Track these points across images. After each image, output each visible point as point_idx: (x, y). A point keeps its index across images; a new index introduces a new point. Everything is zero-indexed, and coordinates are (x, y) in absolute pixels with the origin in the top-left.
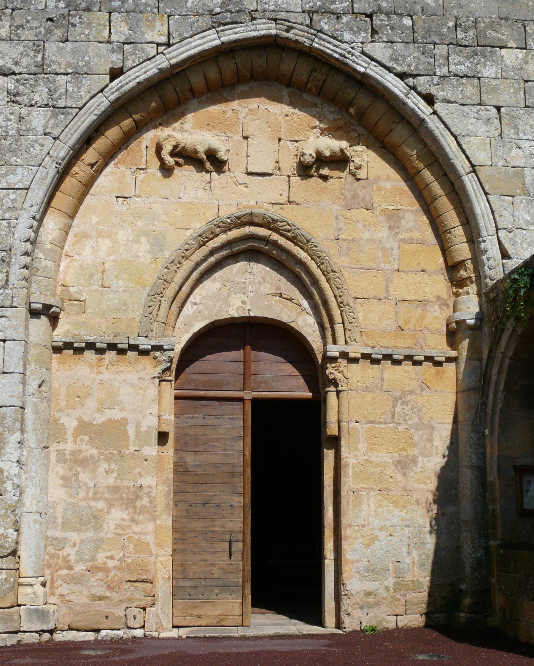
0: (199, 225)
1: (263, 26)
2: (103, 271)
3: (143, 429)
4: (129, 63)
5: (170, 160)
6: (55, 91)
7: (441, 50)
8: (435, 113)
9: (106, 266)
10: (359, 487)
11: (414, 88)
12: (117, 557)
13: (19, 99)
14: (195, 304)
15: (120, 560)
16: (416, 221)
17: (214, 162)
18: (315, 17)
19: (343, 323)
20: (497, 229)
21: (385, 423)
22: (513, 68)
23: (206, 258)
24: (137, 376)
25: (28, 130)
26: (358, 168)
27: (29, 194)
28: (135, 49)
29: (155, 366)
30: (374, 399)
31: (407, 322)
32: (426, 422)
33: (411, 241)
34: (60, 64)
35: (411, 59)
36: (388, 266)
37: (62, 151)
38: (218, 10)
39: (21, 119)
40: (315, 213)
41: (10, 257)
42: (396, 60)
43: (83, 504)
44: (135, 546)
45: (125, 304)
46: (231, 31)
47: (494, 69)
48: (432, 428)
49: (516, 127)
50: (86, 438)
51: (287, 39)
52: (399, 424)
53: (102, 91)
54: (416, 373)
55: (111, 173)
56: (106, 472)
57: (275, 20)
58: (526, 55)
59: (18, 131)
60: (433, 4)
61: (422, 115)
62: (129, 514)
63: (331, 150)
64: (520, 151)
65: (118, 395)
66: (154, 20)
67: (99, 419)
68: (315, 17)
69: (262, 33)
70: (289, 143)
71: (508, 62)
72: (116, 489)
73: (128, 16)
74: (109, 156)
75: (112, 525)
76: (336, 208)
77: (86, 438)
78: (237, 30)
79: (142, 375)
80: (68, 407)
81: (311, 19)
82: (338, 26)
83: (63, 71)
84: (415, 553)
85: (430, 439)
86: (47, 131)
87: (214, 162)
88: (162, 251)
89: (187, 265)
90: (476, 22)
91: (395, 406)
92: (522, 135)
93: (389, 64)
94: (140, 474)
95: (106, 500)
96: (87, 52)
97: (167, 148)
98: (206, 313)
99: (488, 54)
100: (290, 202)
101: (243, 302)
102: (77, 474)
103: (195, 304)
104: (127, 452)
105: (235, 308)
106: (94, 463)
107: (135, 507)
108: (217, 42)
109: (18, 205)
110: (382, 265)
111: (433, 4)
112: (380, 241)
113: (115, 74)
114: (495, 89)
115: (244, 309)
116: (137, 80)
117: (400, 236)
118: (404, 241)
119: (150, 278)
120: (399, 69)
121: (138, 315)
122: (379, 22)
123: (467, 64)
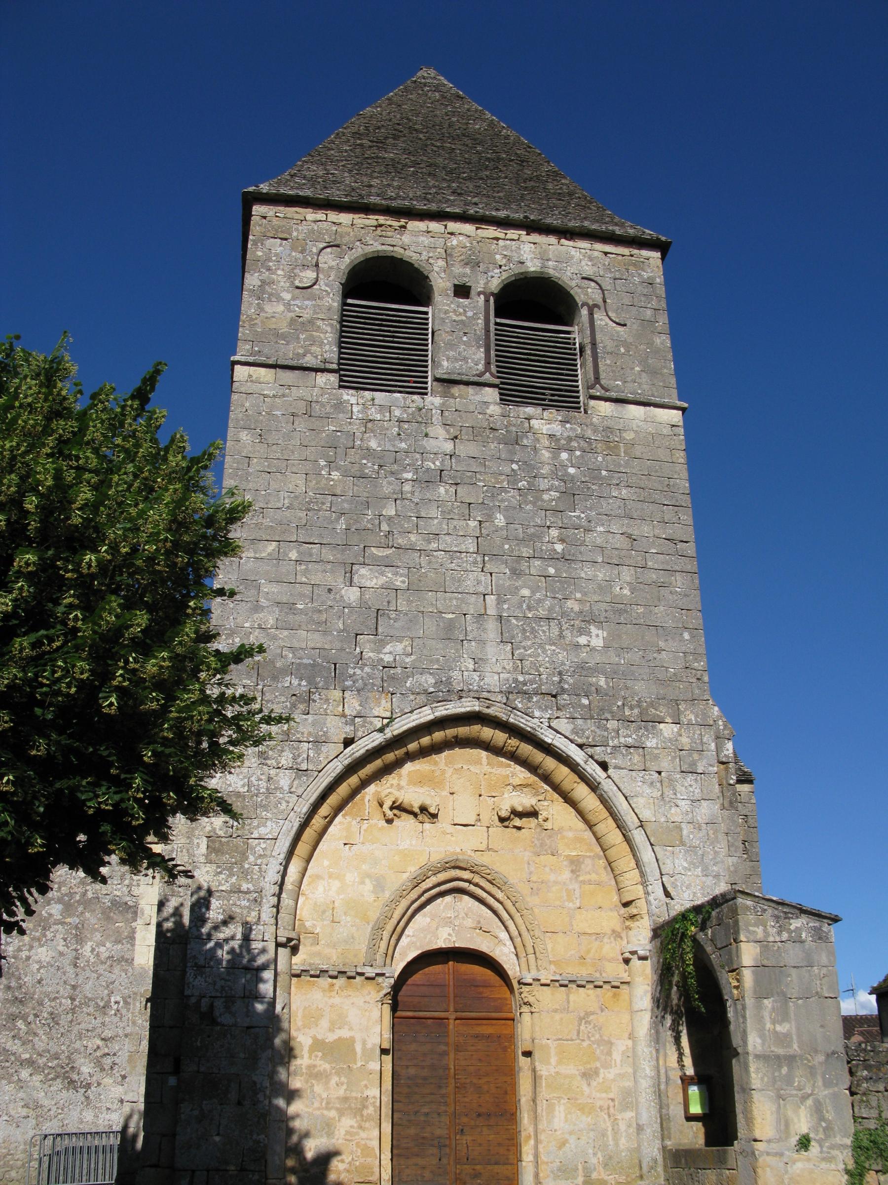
0: (412, 869)
1: (469, 704)
2: (333, 908)
3: (369, 1046)
4: (360, 734)
5: (390, 814)
6: (299, 756)
7: (612, 724)
8: (609, 777)
9: (336, 904)
10: (551, 1096)
11: (591, 757)
12: (347, 1161)
13: (269, 762)
14: (408, 936)
15: (350, 1163)
16: (593, 865)
17: (425, 813)
18: (511, 697)
19: (535, 953)
20: (662, 875)
21: (572, 1040)
22: (670, 740)
23: (419, 897)
24: (363, 1000)
25: (276, 789)
26: (546, 820)
27: (277, 844)
28: (365, 722)
29: (378, 992)
30: (562, 1019)
31: (588, 951)
32: (606, 1038)
33: (590, 882)
34: (303, 733)
35: (590, 731)
36: (571, 905)
37: (304, 808)
38: (432, 690)
39: (269, 779)
40: (509, 857)
41: (262, 897)
42: (577, 733)
43: (318, 1113)
44: (362, 1150)
45: (353, 938)
46: (442, 708)
47: (655, 741)
48: (611, 1044)
49: (674, 789)
50: (320, 1054)
51: (488, 715)
52: (583, 1040)
53: (336, 757)
54: (597, 996)
55: (340, 823)
56: (337, 1085)
57: (478, 699)
58: (680, 729)
59: (268, 789)
60: (605, 686)
61: (598, 779)
62: (357, 1121)
63: (523, 807)
64: (678, 809)
65: (347, 1017)
66: (380, 698)
67: (331, 1037)
68: (511, 697)
69: (468, 709)
70: (488, 799)
71: (666, 734)
72: (345, 1099)
73: (359, 693)
74: (338, 810)
75: (343, 1132)
76: (527, 854)
77: (320, 1054)
78: (447, 707)
79: (368, 998)
80: (304, 1026)
81: (508, 698)
82: (530, 705)
83: (305, 739)
84: (599, 1155)
85: (609, 1053)
86: (292, 790)
87: (425, 813)
88: (383, 891)
89: (404, 903)
90: (639, 701)
91: (580, 1025)
92: (679, 795)
93: (571, 737)
94: (366, 1086)
95: (337, 1109)
96: (325, 724)
97: (388, 804)
98: (418, 944)
99: (650, 728)
100: (489, 849)
101: (450, 935)
102: (313, 1085)
103: (408, 936)
104: (355, 1067)
105: (443, 940)
106: (327, 1077)
107: (362, 1116)
108: (431, 717)
109: (268, 853)
110: (567, 903)
111: (605, 686)
112: (564, 883)
113: (348, 742)
114: (656, 757)
115: (450, 940)
116: (366, 748)
117: (581, 878)
118: (583, 882)
119: (374, 915)
120: (580, 741)
121: (363, 948)
122: (563, 702)
123: (634, 736)
